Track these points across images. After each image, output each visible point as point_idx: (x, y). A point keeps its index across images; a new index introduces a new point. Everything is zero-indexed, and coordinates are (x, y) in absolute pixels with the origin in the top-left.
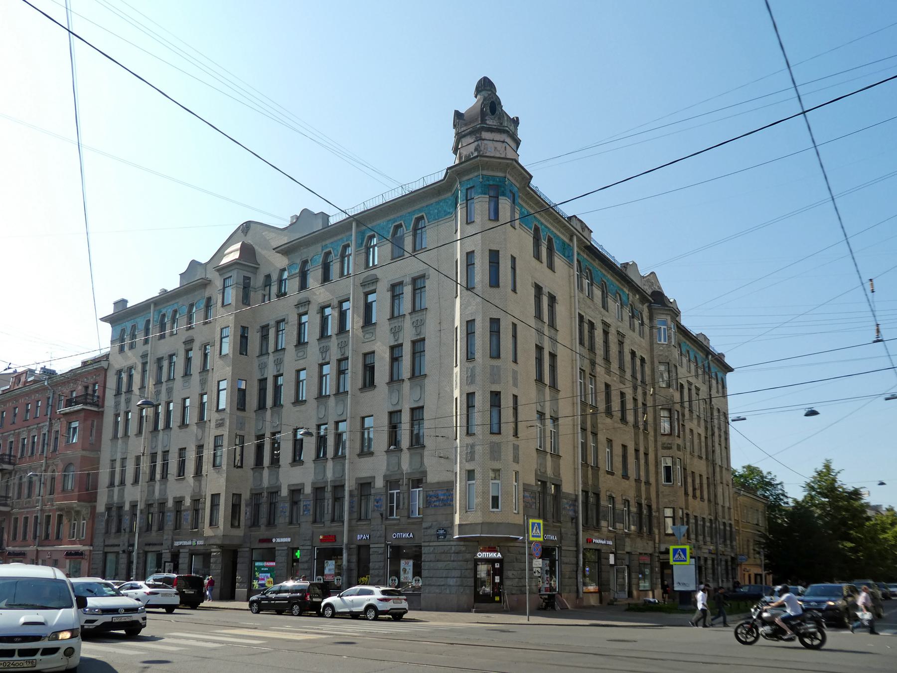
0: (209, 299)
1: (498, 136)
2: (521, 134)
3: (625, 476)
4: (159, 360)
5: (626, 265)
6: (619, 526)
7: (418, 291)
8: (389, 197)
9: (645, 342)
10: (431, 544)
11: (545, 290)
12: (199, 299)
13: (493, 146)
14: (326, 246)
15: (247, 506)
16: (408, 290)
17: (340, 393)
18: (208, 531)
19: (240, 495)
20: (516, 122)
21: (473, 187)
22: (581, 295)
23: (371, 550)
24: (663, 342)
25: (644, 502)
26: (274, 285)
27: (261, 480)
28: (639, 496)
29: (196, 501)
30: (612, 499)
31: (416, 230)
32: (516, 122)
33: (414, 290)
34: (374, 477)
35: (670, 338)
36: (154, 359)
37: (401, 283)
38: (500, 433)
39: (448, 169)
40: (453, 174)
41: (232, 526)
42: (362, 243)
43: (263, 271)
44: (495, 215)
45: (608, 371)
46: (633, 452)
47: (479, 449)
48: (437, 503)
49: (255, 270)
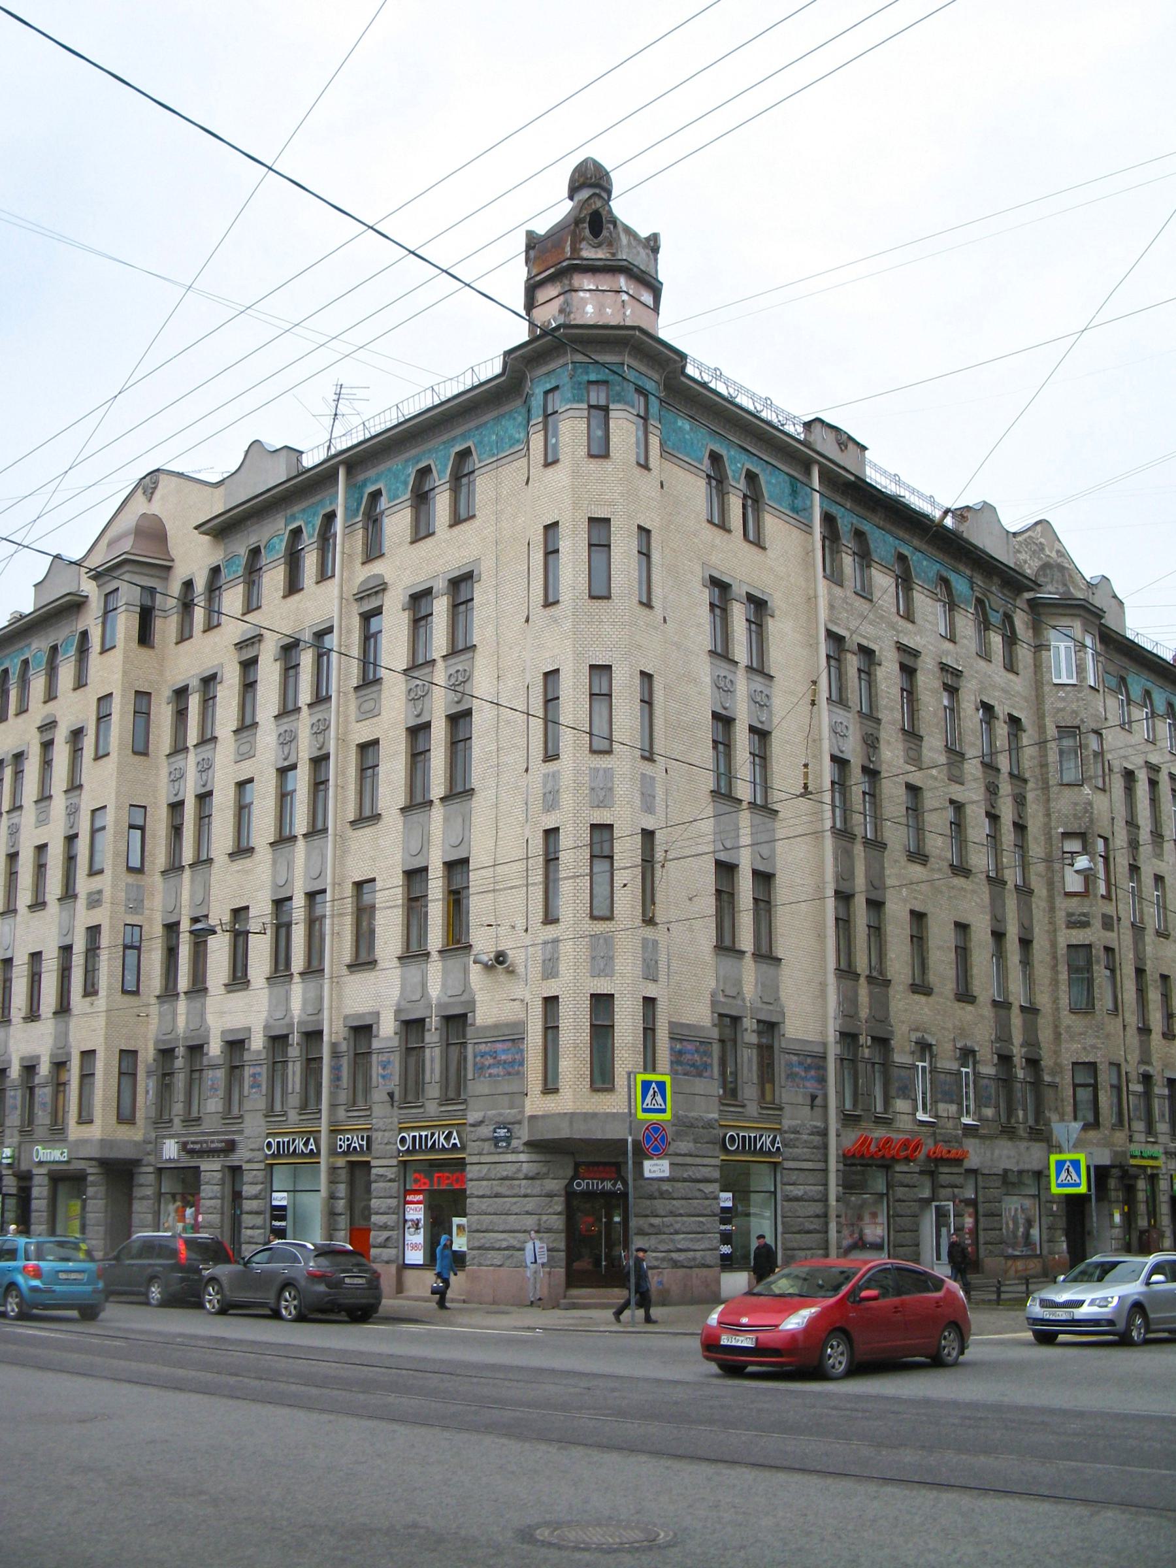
0: (85, 635)
1: (605, 281)
2: (664, 273)
3: (965, 996)
4: (181, 693)
5: (962, 514)
6: (947, 1109)
7: (462, 608)
8: (450, 390)
9: (1019, 684)
10: (484, 1159)
11: (740, 590)
12: (64, 634)
13: (594, 304)
14: (293, 518)
15: (149, 1074)
16: (440, 607)
17: (316, 831)
18: (74, 1131)
19: (135, 1052)
20: (652, 244)
21: (556, 388)
22: (837, 590)
23: (374, 1171)
24: (1064, 680)
25: (1018, 1052)
26: (197, 604)
27: (174, 1019)
28: (1003, 1036)
29: (60, 1066)
30: (924, 1048)
31: (460, 477)
32: (652, 244)
33: (455, 606)
34: (378, 1014)
35: (1081, 669)
36: (167, 693)
37: (428, 592)
38: (610, 918)
39: (507, 353)
40: (522, 363)
41: (121, 1120)
42: (358, 510)
43: (180, 573)
44: (600, 451)
45: (915, 759)
46: (988, 938)
47: (567, 949)
48: (493, 1071)
49: (166, 570)
